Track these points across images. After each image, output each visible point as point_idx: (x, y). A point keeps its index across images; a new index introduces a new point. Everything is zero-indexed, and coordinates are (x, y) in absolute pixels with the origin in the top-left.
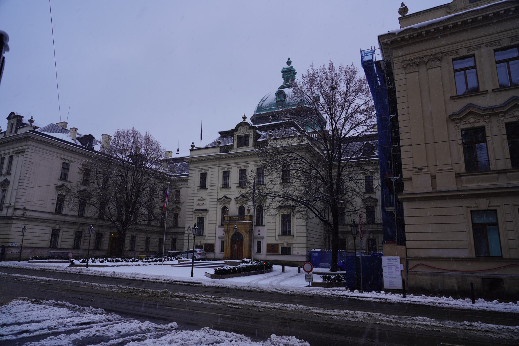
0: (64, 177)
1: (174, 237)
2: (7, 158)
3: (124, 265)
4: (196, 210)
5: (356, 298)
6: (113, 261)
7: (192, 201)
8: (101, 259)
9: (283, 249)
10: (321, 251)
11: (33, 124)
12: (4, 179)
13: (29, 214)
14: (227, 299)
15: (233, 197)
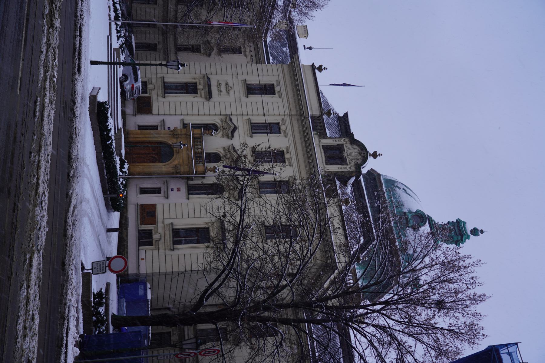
1: (160, 47)
4: (209, 79)
5: (64, 349)
7: (224, 71)
9: (149, 234)
10: (148, 301)
14: (51, 103)
15: (236, 142)
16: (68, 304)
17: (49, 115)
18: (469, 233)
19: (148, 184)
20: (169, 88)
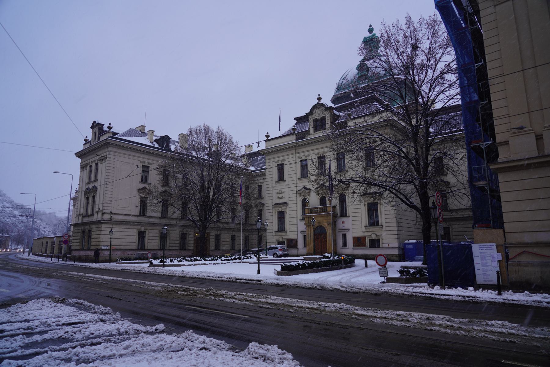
0: (145, 179)
2: (94, 165)
3: (202, 264)
4: (276, 204)
6: (191, 260)
7: (270, 195)
8: (179, 259)
11: (111, 130)
12: (93, 185)
13: (115, 217)
16: (403, 292)
17: (274, 300)
18: (371, 34)
19: (340, 241)
20: (281, 229)
